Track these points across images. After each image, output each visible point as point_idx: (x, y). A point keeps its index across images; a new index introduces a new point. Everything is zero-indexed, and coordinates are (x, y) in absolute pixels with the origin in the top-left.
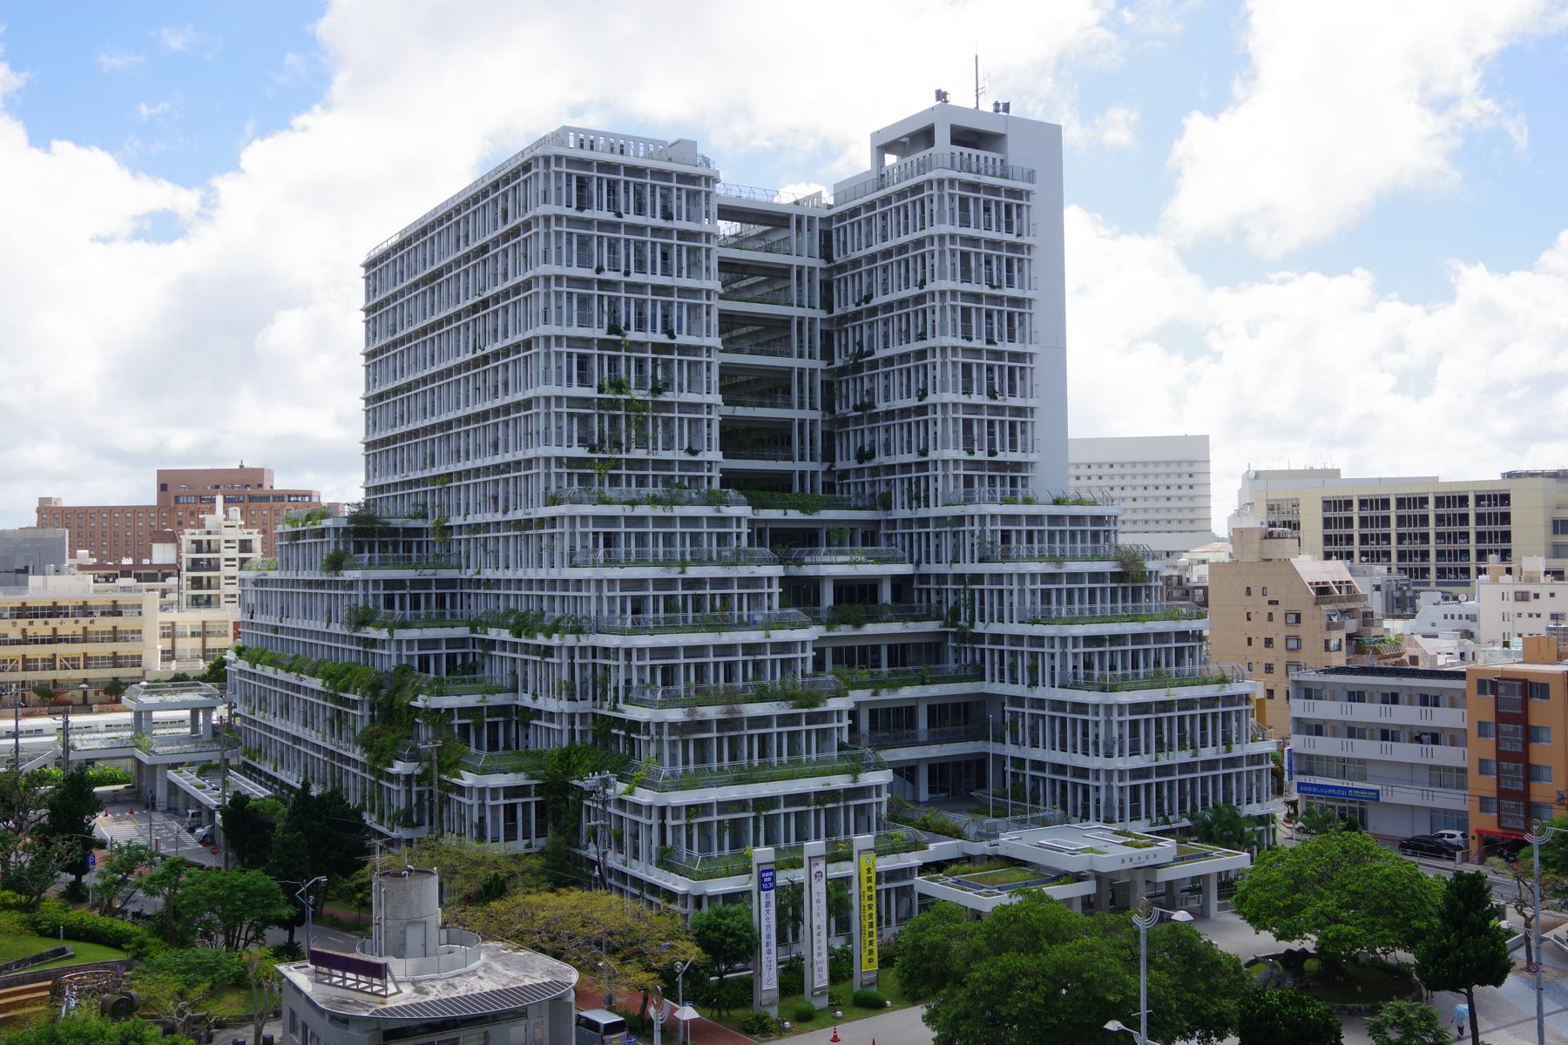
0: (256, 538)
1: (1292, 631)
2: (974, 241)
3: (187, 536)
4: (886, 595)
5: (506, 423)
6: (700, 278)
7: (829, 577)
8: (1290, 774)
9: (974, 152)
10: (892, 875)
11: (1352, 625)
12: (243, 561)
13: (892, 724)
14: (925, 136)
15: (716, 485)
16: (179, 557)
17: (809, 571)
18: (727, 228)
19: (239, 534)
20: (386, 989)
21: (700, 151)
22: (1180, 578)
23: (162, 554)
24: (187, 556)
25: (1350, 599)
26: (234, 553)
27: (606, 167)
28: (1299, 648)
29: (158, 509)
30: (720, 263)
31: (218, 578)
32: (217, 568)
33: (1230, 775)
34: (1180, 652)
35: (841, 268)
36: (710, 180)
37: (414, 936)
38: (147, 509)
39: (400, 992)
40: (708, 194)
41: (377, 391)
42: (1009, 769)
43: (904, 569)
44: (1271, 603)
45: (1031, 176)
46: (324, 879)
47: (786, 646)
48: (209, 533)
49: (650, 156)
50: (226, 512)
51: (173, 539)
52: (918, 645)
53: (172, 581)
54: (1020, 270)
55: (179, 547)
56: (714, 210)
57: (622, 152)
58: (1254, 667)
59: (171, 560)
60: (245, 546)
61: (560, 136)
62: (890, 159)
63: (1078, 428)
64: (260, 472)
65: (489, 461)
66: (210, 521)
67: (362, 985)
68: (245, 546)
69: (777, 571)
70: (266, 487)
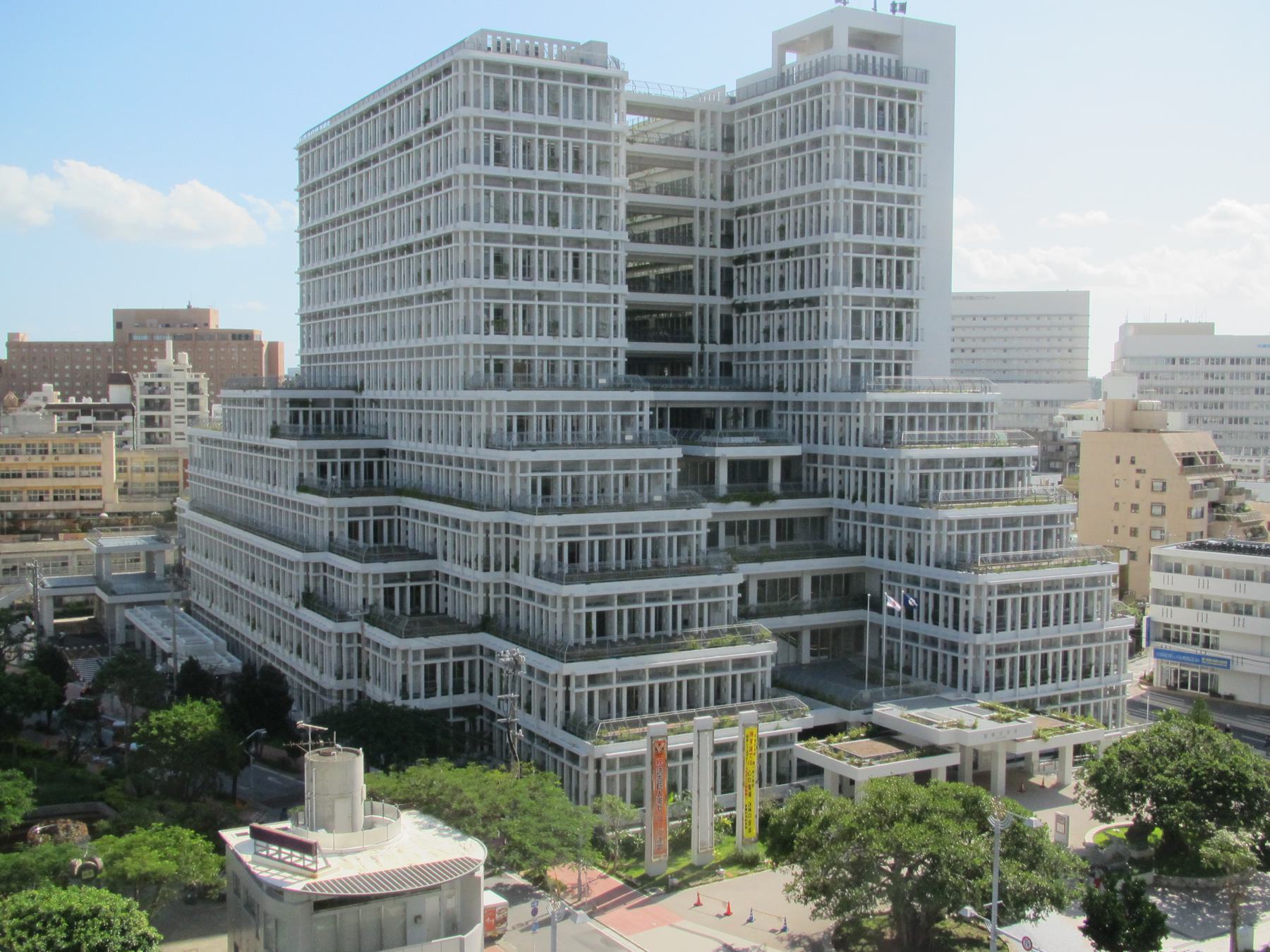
0: (203, 381)
1: (1158, 498)
2: (868, 142)
3: (140, 379)
4: (776, 475)
5: (429, 309)
6: (609, 175)
7: (724, 457)
8: (1148, 640)
9: (870, 53)
10: (773, 741)
11: (1214, 494)
12: (191, 417)
13: (777, 597)
14: (826, 36)
15: (621, 370)
16: (133, 398)
17: (706, 452)
18: (632, 120)
19: (189, 377)
20: (316, 862)
21: (610, 52)
22: (1055, 434)
23: (117, 394)
24: (141, 397)
25: (1214, 470)
26: (184, 411)
27: (521, 70)
28: (1163, 513)
29: (114, 345)
30: (628, 157)
31: (168, 417)
32: (168, 409)
33: (1088, 706)
34: (1048, 533)
35: (741, 308)
36: (621, 80)
37: (341, 808)
38: (105, 345)
39: (328, 866)
40: (617, 94)
41: (310, 181)
42: (884, 637)
43: (794, 450)
44: (1139, 471)
45: (923, 77)
46: (263, 731)
47: (682, 525)
48: (160, 376)
49: (562, 57)
50: (175, 357)
51: (126, 380)
52: (805, 520)
53: (127, 419)
54: (911, 167)
55: (133, 389)
56: (623, 108)
57: (537, 54)
58: (1120, 529)
59: (127, 401)
60: (193, 388)
61: (477, 41)
62: (791, 58)
63: (960, 284)
64: (206, 312)
65: (413, 343)
66: (161, 365)
67: (294, 859)
68: (193, 388)
69: (676, 452)
70: (212, 326)
